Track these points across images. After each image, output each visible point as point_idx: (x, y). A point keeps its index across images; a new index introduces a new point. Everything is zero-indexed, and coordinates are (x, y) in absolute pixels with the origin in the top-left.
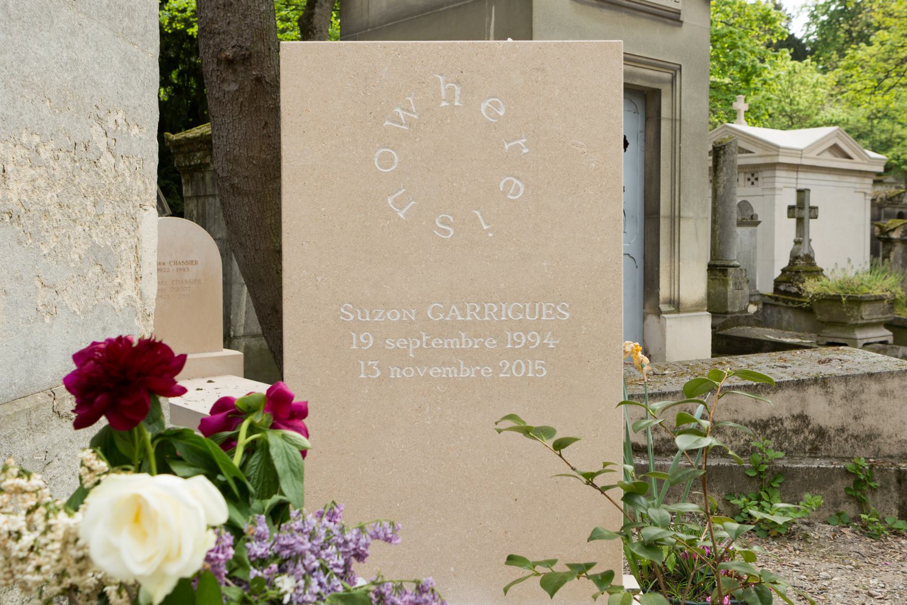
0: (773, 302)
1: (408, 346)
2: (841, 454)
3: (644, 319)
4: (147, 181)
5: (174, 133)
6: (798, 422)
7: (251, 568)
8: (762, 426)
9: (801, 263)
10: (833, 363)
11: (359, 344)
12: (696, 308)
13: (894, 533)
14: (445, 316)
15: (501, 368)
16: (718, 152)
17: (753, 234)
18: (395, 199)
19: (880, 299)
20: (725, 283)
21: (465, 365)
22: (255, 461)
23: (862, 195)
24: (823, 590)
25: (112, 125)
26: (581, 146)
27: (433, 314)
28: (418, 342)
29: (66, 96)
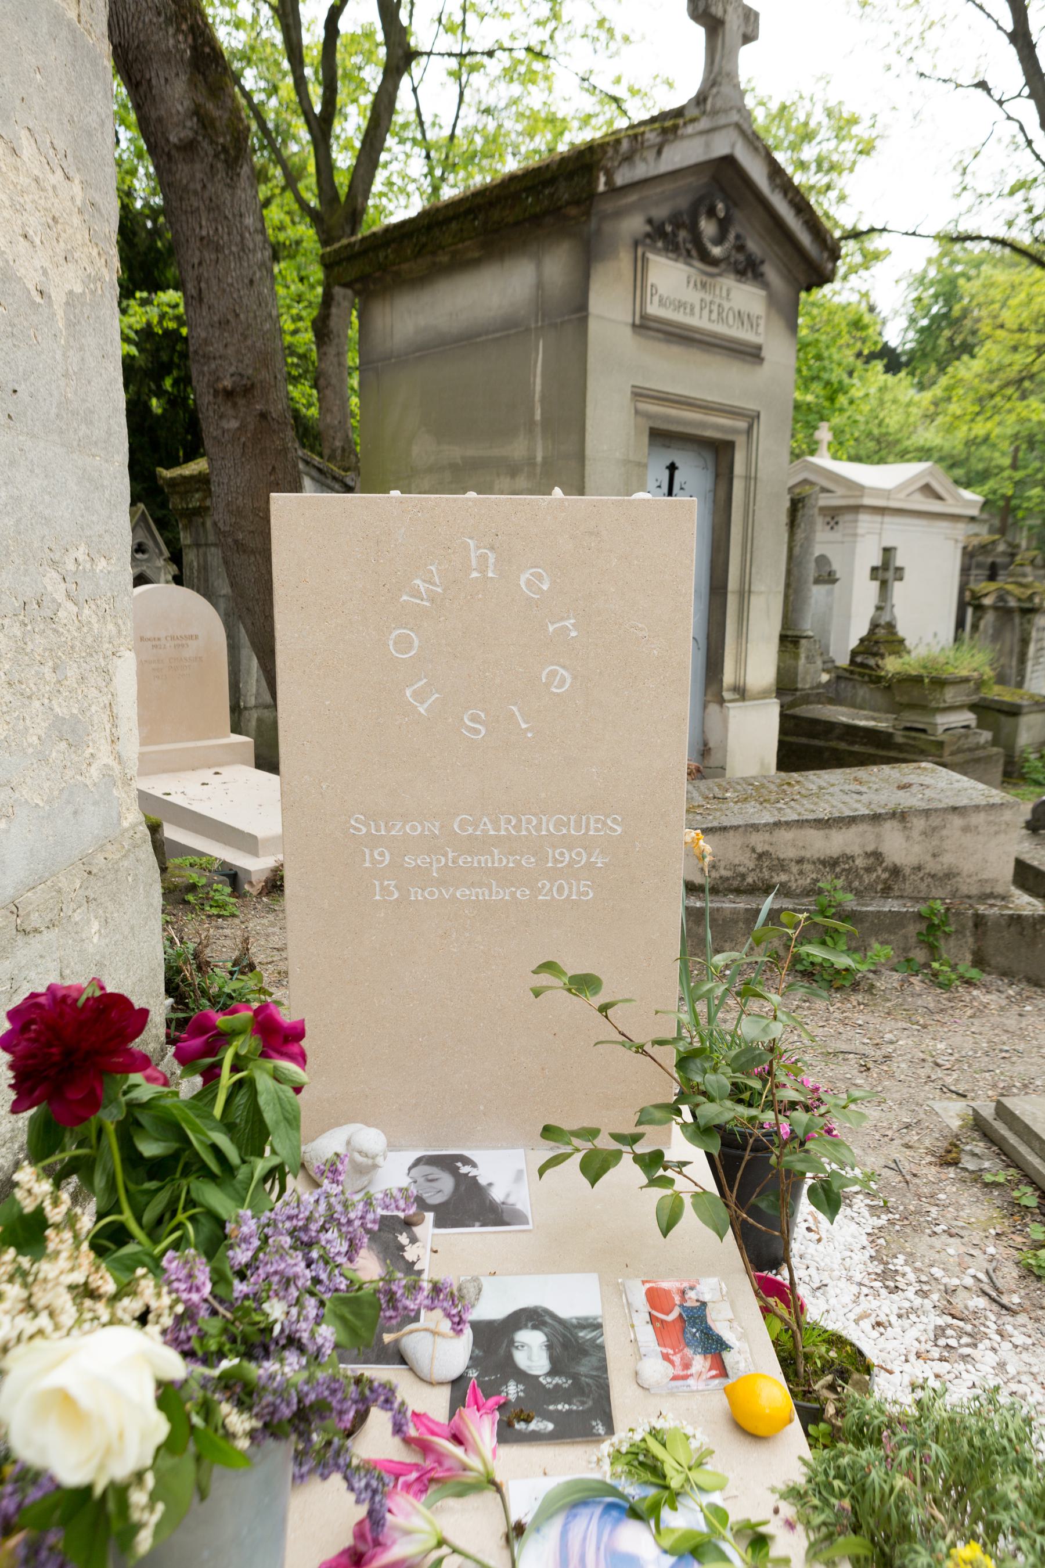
0: (847, 675)
1: (431, 864)
2: (915, 894)
3: (705, 707)
4: (120, 622)
5: (167, 468)
6: (872, 860)
7: (236, 1282)
8: (831, 863)
9: (881, 632)
10: (914, 789)
11: (373, 861)
12: (763, 695)
13: (967, 982)
14: (475, 830)
15: (540, 890)
16: (796, 506)
17: (830, 593)
18: (414, 692)
19: (966, 680)
20: (796, 657)
21: (498, 886)
22: (241, 1099)
23: (952, 542)
24: (887, 1057)
25: (71, 566)
26: (642, 629)
27: (460, 827)
28: (443, 860)
29: (8, 546)
